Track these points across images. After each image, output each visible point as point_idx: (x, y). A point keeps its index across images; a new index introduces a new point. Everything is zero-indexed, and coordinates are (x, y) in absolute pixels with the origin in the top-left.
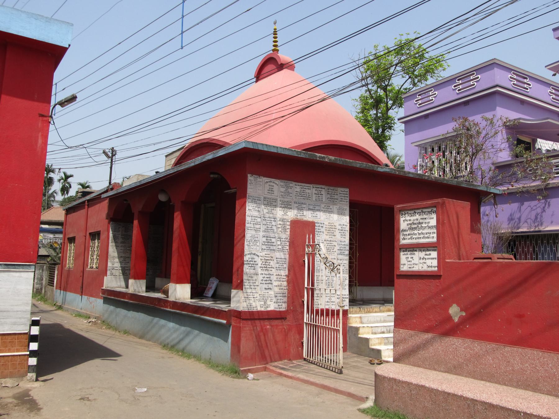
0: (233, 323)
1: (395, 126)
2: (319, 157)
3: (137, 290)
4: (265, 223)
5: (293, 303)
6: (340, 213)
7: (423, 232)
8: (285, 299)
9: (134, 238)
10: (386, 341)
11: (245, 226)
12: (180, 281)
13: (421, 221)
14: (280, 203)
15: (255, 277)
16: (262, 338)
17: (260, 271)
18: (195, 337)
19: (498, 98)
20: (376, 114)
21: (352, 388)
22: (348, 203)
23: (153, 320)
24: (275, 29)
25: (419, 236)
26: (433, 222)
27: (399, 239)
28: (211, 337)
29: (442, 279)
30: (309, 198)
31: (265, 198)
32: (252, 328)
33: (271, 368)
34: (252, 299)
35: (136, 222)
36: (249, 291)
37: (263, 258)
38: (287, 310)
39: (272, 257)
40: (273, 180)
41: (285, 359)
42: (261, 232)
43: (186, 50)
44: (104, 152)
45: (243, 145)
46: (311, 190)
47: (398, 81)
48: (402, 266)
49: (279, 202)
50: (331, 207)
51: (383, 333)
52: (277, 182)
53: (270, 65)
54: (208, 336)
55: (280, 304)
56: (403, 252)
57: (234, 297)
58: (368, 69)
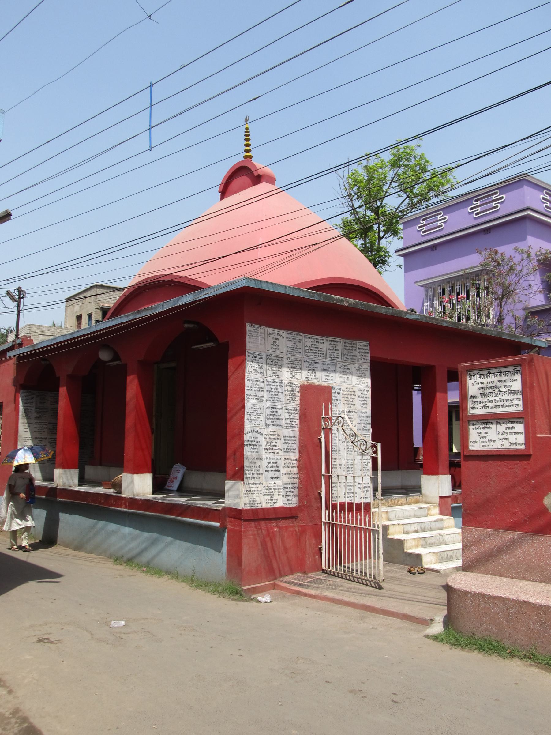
0: (229, 526)
1: (390, 261)
2: (337, 300)
3: (67, 483)
4: (268, 386)
5: (307, 495)
6: (360, 375)
7: (503, 398)
8: (296, 492)
9: (61, 412)
10: (424, 542)
11: (244, 393)
12: (138, 470)
13: (499, 384)
14: (287, 361)
15: (258, 463)
16: (269, 544)
17: (264, 455)
18: (167, 546)
19: (528, 225)
20: (365, 244)
21: (407, 608)
22: (369, 361)
23: (96, 524)
24: (247, 129)
25: (497, 404)
26: (517, 385)
27: (466, 408)
28: (194, 546)
29: (532, 460)
30: (321, 355)
31: (268, 355)
32: (256, 532)
33: (283, 585)
34: (256, 492)
35: (63, 391)
36: (251, 481)
37: (267, 437)
38: (299, 506)
39: (279, 435)
40: (277, 331)
41: (297, 571)
42: (265, 402)
43: (157, 152)
44: (8, 293)
45: (243, 284)
46: (324, 344)
47: (393, 202)
48: (471, 444)
49: (286, 361)
50: (349, 367)
51: (417, 531)
52: (282, 334)
53: (243, 175)
54: (189, 545)
55: (290, 498)
56: (473, 425)
57: (228, 490)
58: (355, 185)
